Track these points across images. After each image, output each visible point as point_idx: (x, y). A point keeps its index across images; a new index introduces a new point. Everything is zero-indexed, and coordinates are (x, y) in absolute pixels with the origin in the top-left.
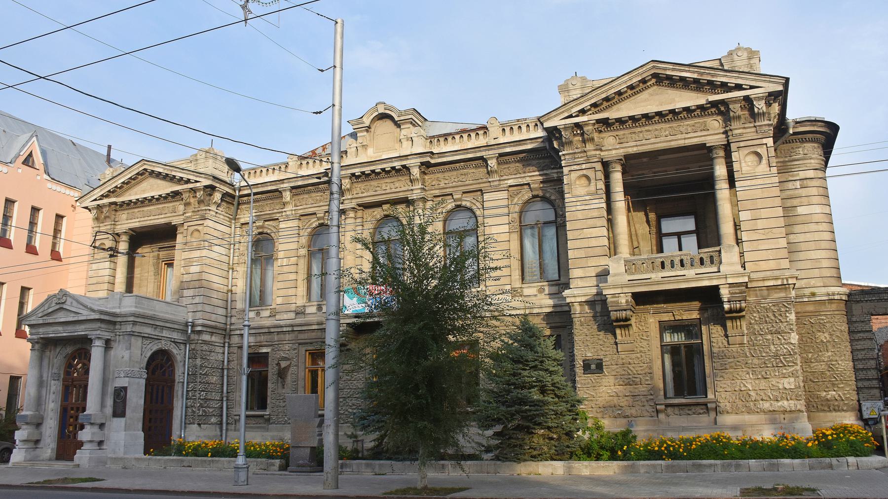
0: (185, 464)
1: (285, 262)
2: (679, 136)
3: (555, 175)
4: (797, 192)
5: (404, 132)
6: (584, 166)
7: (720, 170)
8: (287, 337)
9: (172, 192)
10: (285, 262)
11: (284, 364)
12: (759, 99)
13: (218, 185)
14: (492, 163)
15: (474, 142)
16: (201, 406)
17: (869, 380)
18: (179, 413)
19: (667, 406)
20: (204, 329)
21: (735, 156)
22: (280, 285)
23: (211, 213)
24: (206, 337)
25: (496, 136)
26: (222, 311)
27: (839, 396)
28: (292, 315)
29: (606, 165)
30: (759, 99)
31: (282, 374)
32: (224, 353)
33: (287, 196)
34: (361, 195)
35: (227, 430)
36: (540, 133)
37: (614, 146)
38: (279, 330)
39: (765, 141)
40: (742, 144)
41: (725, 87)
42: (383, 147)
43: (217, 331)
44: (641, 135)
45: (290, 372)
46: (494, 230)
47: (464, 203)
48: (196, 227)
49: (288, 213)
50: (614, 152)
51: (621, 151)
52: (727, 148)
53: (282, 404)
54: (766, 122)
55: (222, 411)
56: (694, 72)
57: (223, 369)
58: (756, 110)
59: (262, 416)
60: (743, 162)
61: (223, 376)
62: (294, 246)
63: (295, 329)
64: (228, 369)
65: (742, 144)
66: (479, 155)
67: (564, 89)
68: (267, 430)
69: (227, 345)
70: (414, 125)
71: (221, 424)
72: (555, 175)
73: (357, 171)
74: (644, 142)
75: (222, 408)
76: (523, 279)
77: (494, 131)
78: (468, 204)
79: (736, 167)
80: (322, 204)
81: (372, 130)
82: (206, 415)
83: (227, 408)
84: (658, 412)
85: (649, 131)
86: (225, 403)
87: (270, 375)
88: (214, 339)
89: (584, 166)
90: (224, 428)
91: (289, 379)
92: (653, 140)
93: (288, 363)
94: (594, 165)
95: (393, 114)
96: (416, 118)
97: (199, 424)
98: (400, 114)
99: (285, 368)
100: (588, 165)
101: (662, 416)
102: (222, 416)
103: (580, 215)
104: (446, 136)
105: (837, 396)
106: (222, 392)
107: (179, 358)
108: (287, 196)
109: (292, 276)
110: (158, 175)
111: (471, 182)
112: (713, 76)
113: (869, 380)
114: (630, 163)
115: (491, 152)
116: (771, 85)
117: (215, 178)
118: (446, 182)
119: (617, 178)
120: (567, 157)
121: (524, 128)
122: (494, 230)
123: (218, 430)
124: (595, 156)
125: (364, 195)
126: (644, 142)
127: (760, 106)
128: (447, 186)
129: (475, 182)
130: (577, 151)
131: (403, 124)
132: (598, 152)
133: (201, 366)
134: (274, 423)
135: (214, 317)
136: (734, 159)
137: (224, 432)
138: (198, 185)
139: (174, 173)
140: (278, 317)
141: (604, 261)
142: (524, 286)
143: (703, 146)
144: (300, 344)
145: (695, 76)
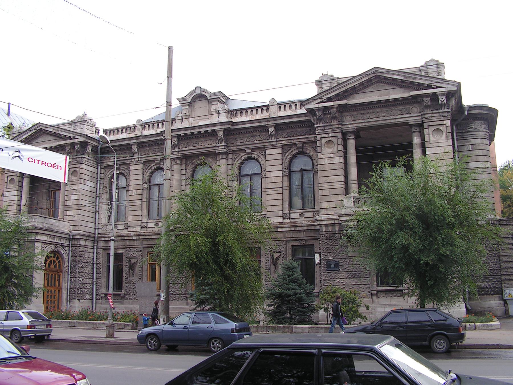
0: (72, 324)
1: (134, 193)
2: (392, 117)
3: (313, 139)
4: (469, 153)
5: (213, 107)
6: (330, 135)
7: (416, 140)
8: (136, 243)
9: (59, 145)
10: (134, 193)
11: (133, 261)
12: (442, 95)
13: (89, 141)
14: (271, 130)
15: (260, 116)
16: (80, 287)
17: (509, 275)
18: (66, 292)
19: (378, 291)
20: (82, 237)
21: (426, 131)
22: (130, 209)
23: (85, 159)
24: (82, 242)
25: (274, 112)
26: (92, 225)
27: (489, 285)
28: (139, 229)
29: (345, 136)
30: (442, 95)
31: (132, 267)
32: (93, 253)
33: (135, 149)
34: (184, 149)
35: (96, 303)
36: (303, 111)
37: (350, 124)
38: (131, 238)
39: (445, 122)
40: (431, 124)
41: (420, 86)
42: (201, 119)
43: (89, 239)
44: (368, 115)
45: (137, 266)
46: (273, 174)
47: (253, 156)
48: (75, 169)
49: (136, 160)
50: (350, 126)
51: (355, 125)
52: (421, 126)
53: (132, 287)
54: (446, 110)
55: (93, 291)
56: (402, 76)
57: (93, 264)
58: (440, 102)
59: (119, 295)
60: (431, 137)
61: (93, 268)
62: (140, 182)
63: (141, 237)
64: (97, 263)
65: (431, 124)
66: (263, 124)
67: (319, 83)
68: (123, 304)
69: (95, 247)
70: (220, 102)
71: (92, 299)
72: (313, 139)
73: (182, 133)
74: (370, 120)
75: (93, 289)
76: (290, 208)
77: (273, 109)
78: (256, 157)
79: (426, 138)
80: (158, 154)
81: (192, 105)
82: (83, 294)
83: (96, 289)
84: (372, 295)
85: (372, 113)
86: (95, 286)
87: (124, 267)
88: (87, 243)
89: (330, 135)
90: (94, 302)
91: (137, 270)
92: (375, 119)
93: (136, 260)
94: (336, 134)
95: (206, 95)
96: (221, 98)
97: (79, 300)
98: (211, 94)
99: (134, 263)
100: (333, 135)
101: (375, 298)
102: (93, 294)
103: (327, 167)
104: (241, 110)
105: (487, 285)
106: (93, 278)
107: (65, 256)
108: (135, 149)
109: (138, 213)
110: (50, 133)
111: (258, 142)
112: (413, 79)
113: (509, 275)
114: (357, 133)
115: (270, 123)
116: (449, 86)
117: (87, 137)
118: (242, 141)
119: (351, 143)
120: (319, 128)
121: (293, 107)
122: (273, 174)
123: (91, 303)
124: (337, 128)
125: (186, 149)
126: (370, 120)
127: (442, 99)
128: (242, 144)
129: (261, 142)
130: (326, 125)
131: (213, 101)
132: (340, 126)
133: (79, 261)
134: (127, 299)
135: (87, 229)
136: (425, 134)
137: (94, 305)
138: (76, 140)
139: (60, 133)
140: (129, 229)
141: (341, 197)
142: (291, 212)
143: (406, 124)
144: (144, 248)
145: (402, 78)
